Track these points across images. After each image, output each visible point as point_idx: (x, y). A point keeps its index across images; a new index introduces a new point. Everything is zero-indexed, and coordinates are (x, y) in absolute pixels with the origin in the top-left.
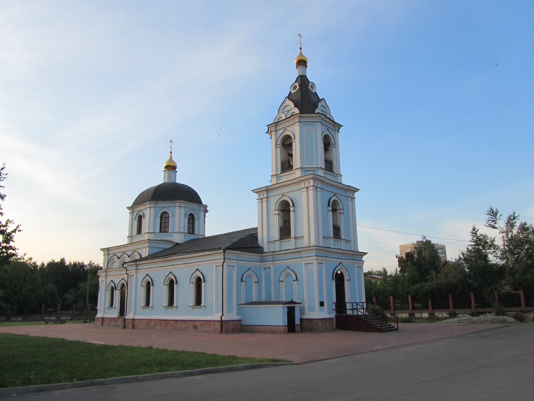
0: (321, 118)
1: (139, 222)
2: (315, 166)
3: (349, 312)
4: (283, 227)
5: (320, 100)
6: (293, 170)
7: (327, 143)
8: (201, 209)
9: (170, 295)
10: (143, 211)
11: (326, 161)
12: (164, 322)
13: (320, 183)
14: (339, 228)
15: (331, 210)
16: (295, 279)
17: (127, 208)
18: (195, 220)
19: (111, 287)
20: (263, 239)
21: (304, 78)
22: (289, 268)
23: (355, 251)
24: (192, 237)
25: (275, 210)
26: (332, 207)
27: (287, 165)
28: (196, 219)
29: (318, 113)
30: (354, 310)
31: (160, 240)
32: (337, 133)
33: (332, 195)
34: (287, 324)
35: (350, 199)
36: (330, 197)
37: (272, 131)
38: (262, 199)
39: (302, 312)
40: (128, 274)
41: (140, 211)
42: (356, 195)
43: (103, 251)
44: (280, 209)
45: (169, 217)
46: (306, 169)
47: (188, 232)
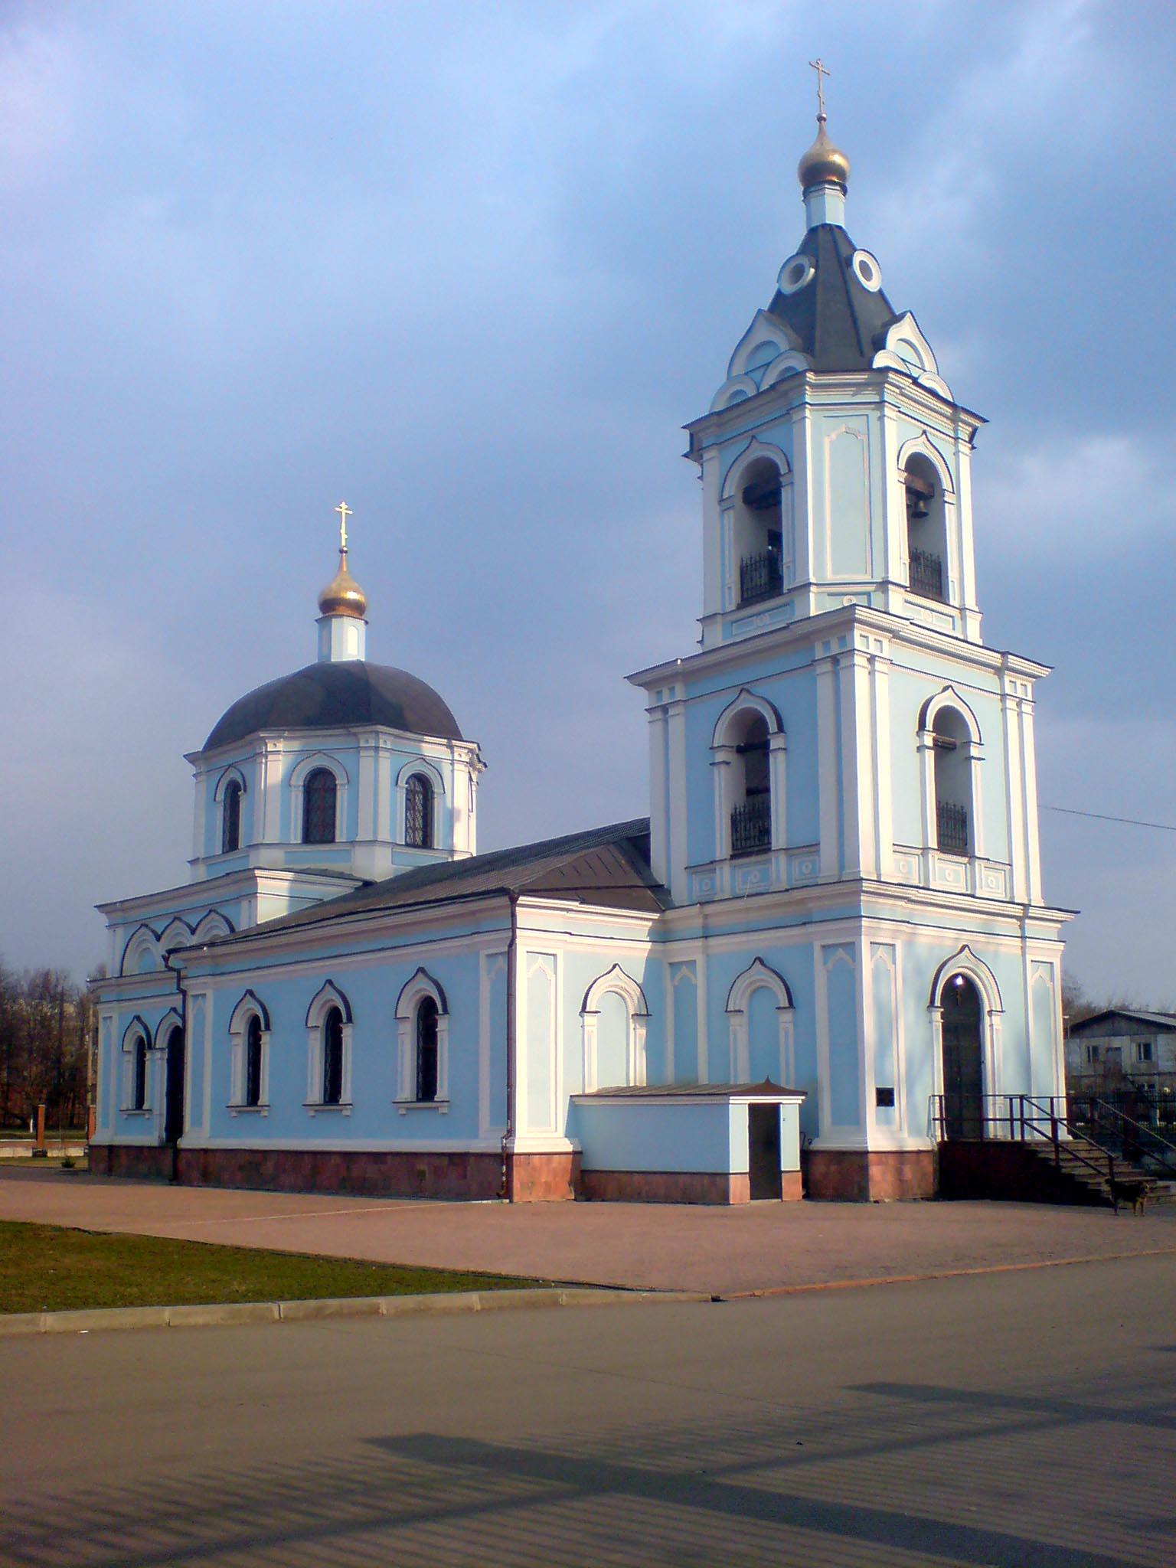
2: (867, 578)
3: (996, 1131)
6: (781, 594)
7: (919, 485)
11: (915, 557)
12: (306, 1157)
13: (885, 642)
16: (784, 1003)
17: (184, 756)
19: (136, 1037)
22: (762, 962)
24: (425, 858)
25: (711, 749)
27: (762, 578)
28: (435, 796)
30: (1009, 1122)
34: (748, 1171)
36: (928, 697)
38: (665, 709)
41: (230, 766)
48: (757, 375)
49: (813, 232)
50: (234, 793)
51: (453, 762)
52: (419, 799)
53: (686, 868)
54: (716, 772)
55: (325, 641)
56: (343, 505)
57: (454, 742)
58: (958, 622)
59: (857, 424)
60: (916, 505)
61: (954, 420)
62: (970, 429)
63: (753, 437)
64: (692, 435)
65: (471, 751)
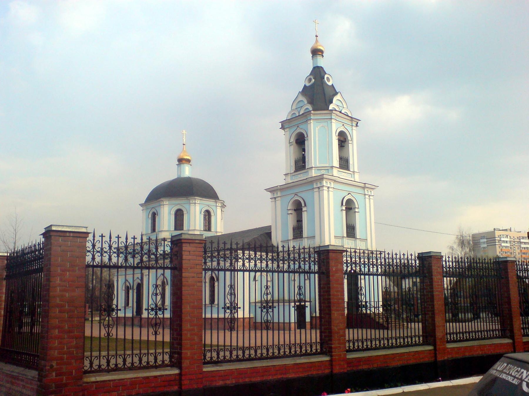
0: (335, 114)
2: (328, 165)
6: (305, 169)
7: (342, 139)
11: (341, 158)
13: (332, 183)
15: (345, 209)
18: (211, 217)
20: (277, 239)
38: (275, 198)
46: (318, 168)
48: (299, 109)
49: (314, 68)
50: (154, 215)
51: (216, 206)
52: (207, 217)
53: (281, 241)
54: (289, 216)
55: (179, 171)
56: (184, 131)
57: (217, 201)
58: (353, 175)
59: (325, 124)
60: (342, 144)
61: (352, 121)
62: (356, 123)
63: (298, 126)
64: (282, 125)
65: (222, 203)
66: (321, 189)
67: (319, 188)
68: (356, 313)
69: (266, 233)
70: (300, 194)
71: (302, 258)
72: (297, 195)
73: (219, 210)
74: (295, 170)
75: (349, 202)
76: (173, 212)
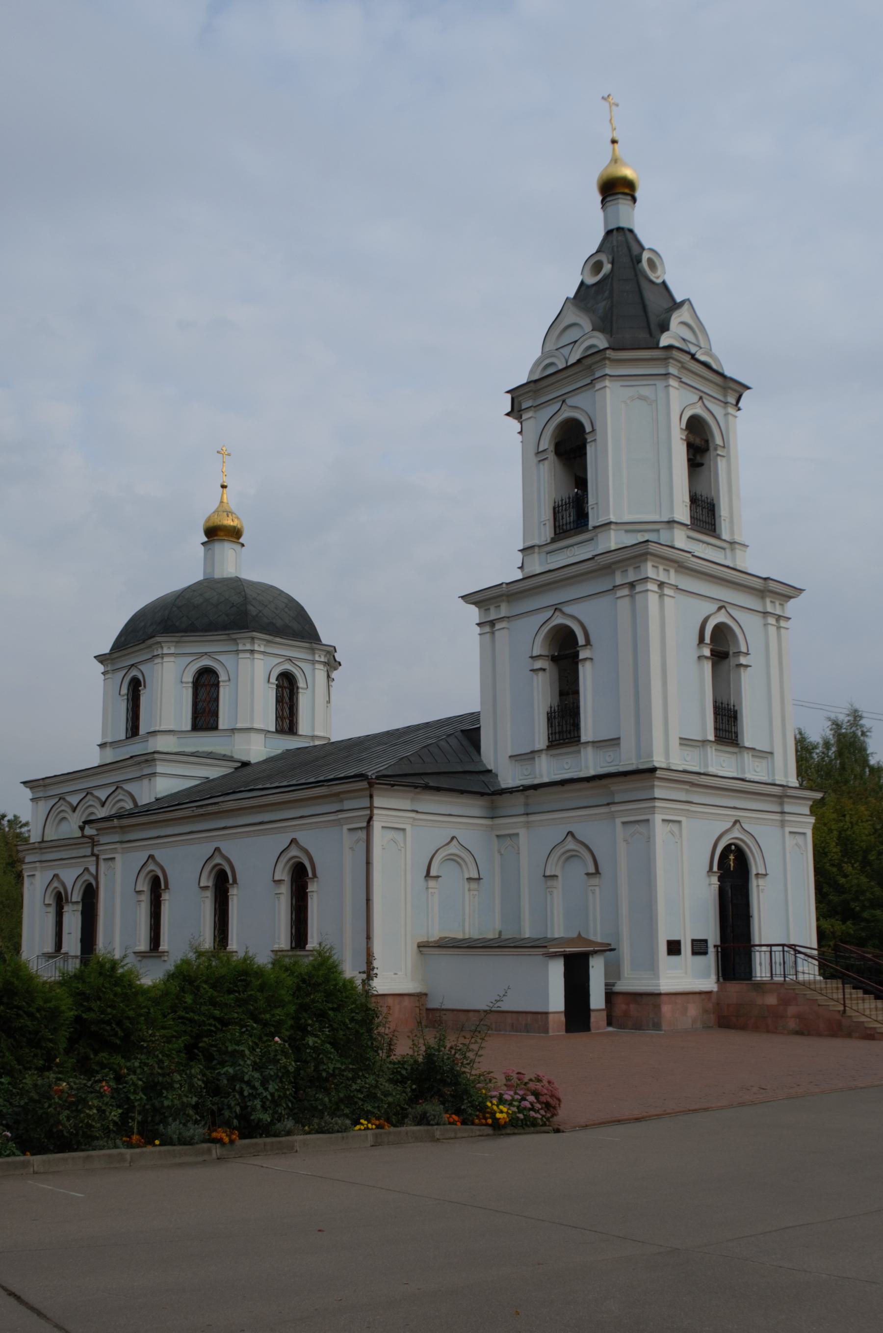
1: (133, 700)
4: (556, 709)
5: (677, 306)
6: (588, 530)
7: (698, 441)
8: (317, 658)
9: (217, 918)
10: (142, 667)
11: (694, 499)
13: (672, 572)
14: (736, 712)
16: (592, 870)
17: (95, 657)
18: (298, 693)
21: (629, 235)
23: (785, 784)
24: (290, 743)
26: (711, 647)
27: (569, 516)
28: (300, 690)
29: (670, 347)
31: (193, 755)
32: (731, 410)
33: (714, 607)
35: (771, 620)
37: (523, 407)
38: (492, 623)
39: (613, 972)
40: (97, 857)
41: (133, 665)
42: (792, 607)
43: (31, 788)
44: (547, 654)
45: (219, 682)
47: (279, 729)
48: (566, 351)
49: (609, 233)
50: (135, 687)
52: (286, 693)
65: (328, 652)
66: (639, 588)
67: (632, 585)
68: (783, 979)
69: (462, 731)
70: (567, 609)
71: (332, 985)
72: (560, 610)
73: (320, 674)
74: (553, 535)
75: (722, 633)
76: (189, 677)
